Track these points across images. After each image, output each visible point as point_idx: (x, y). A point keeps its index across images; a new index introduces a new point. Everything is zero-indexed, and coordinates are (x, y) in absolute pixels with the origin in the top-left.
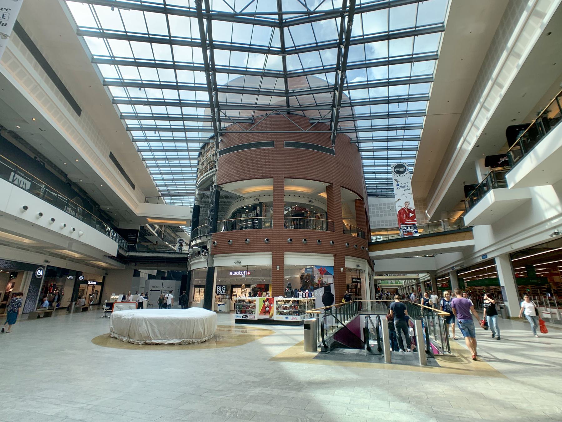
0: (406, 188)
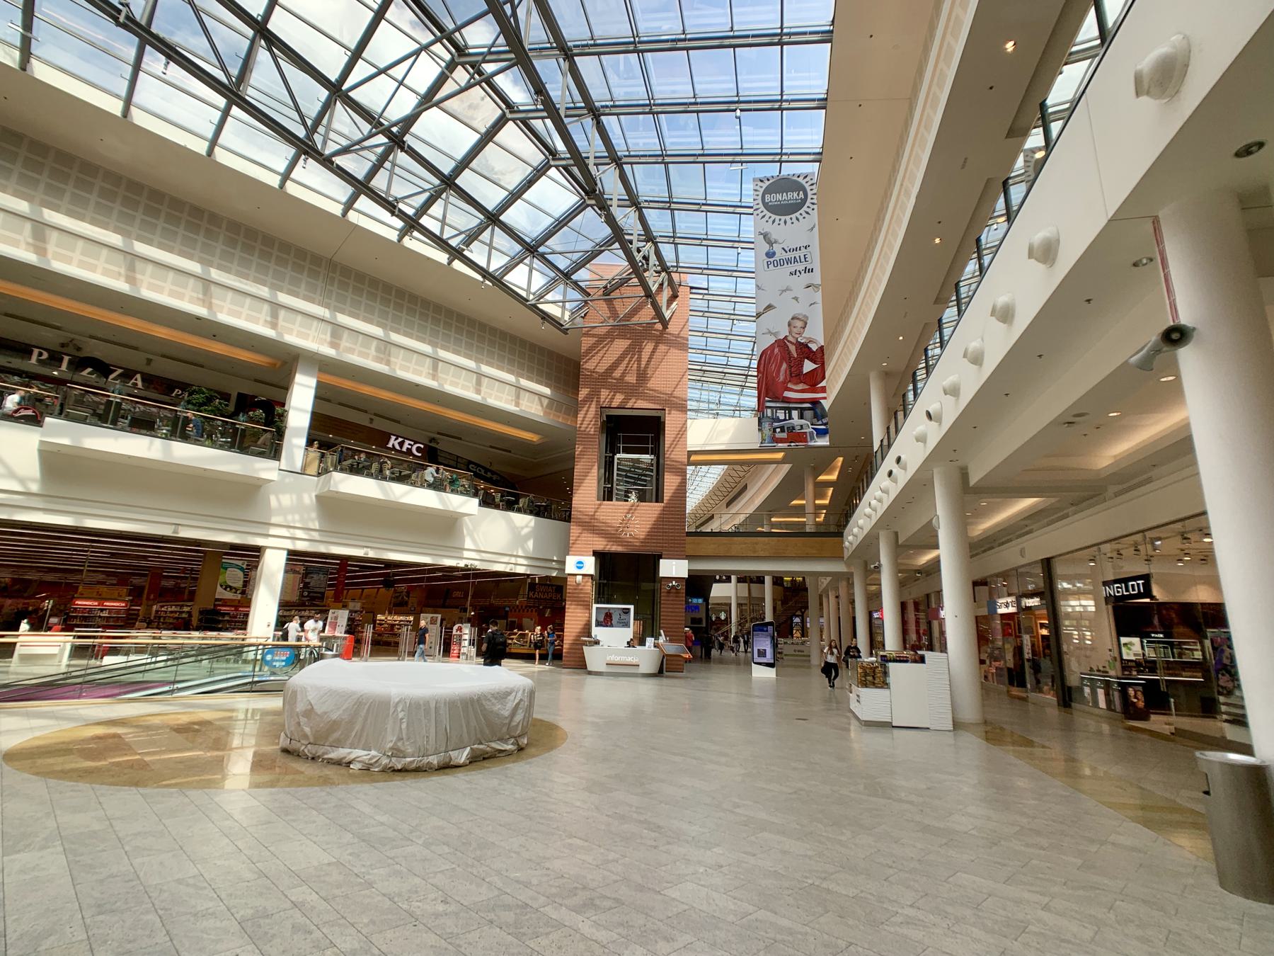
0: (801, 267)
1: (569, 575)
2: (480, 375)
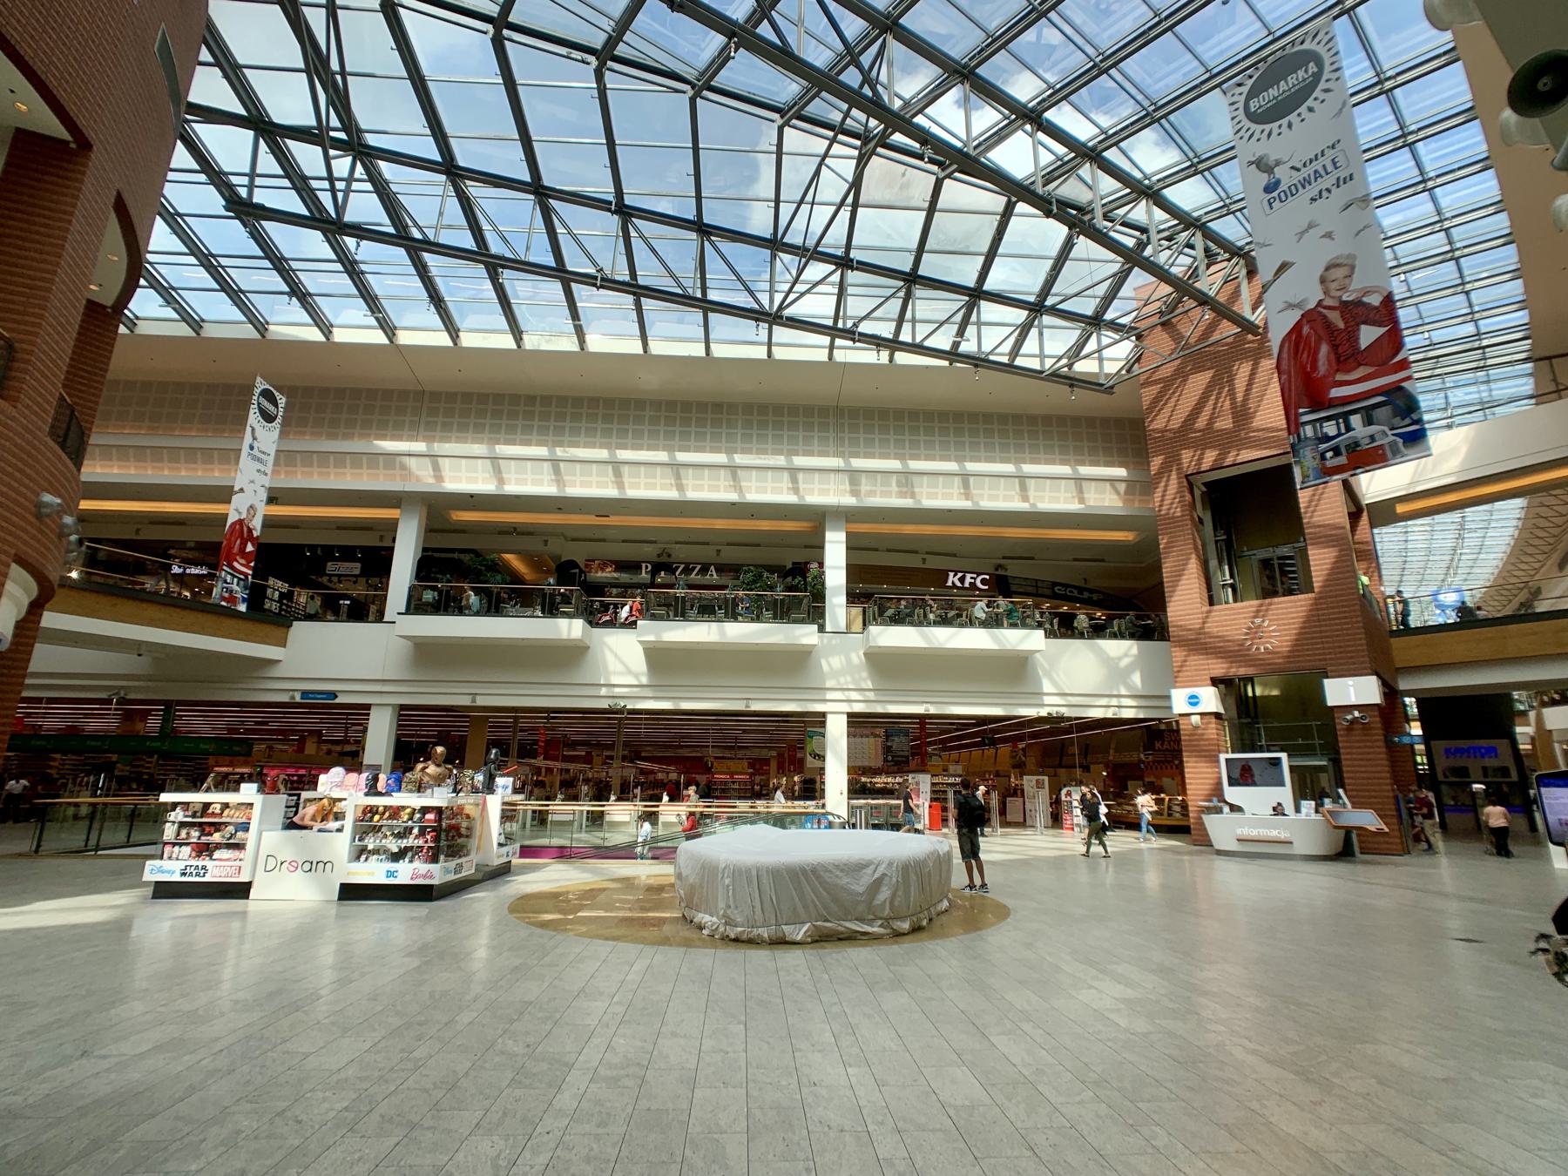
0: (1328, 182)
1: (1180, 715)
2: (1022, 478)
